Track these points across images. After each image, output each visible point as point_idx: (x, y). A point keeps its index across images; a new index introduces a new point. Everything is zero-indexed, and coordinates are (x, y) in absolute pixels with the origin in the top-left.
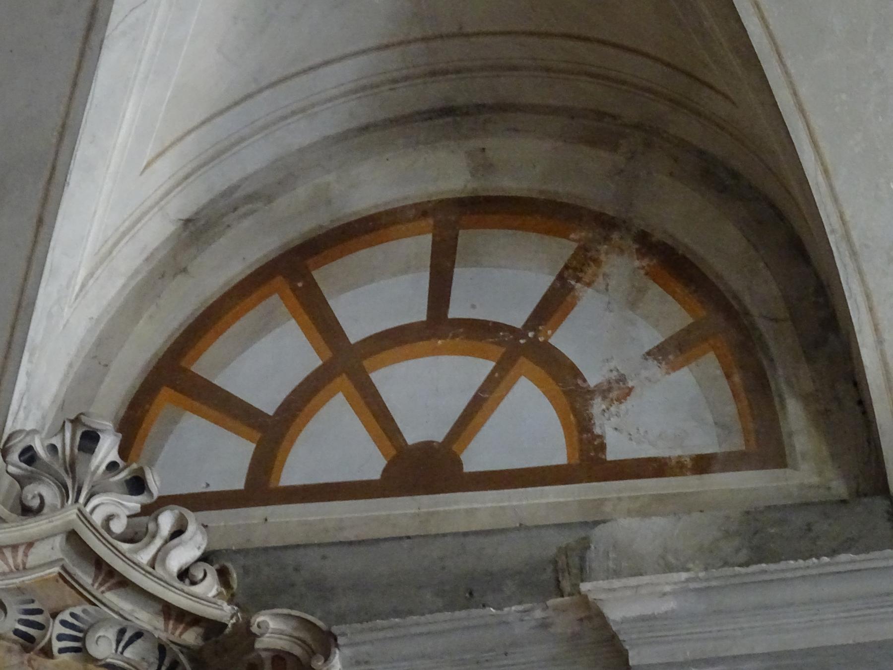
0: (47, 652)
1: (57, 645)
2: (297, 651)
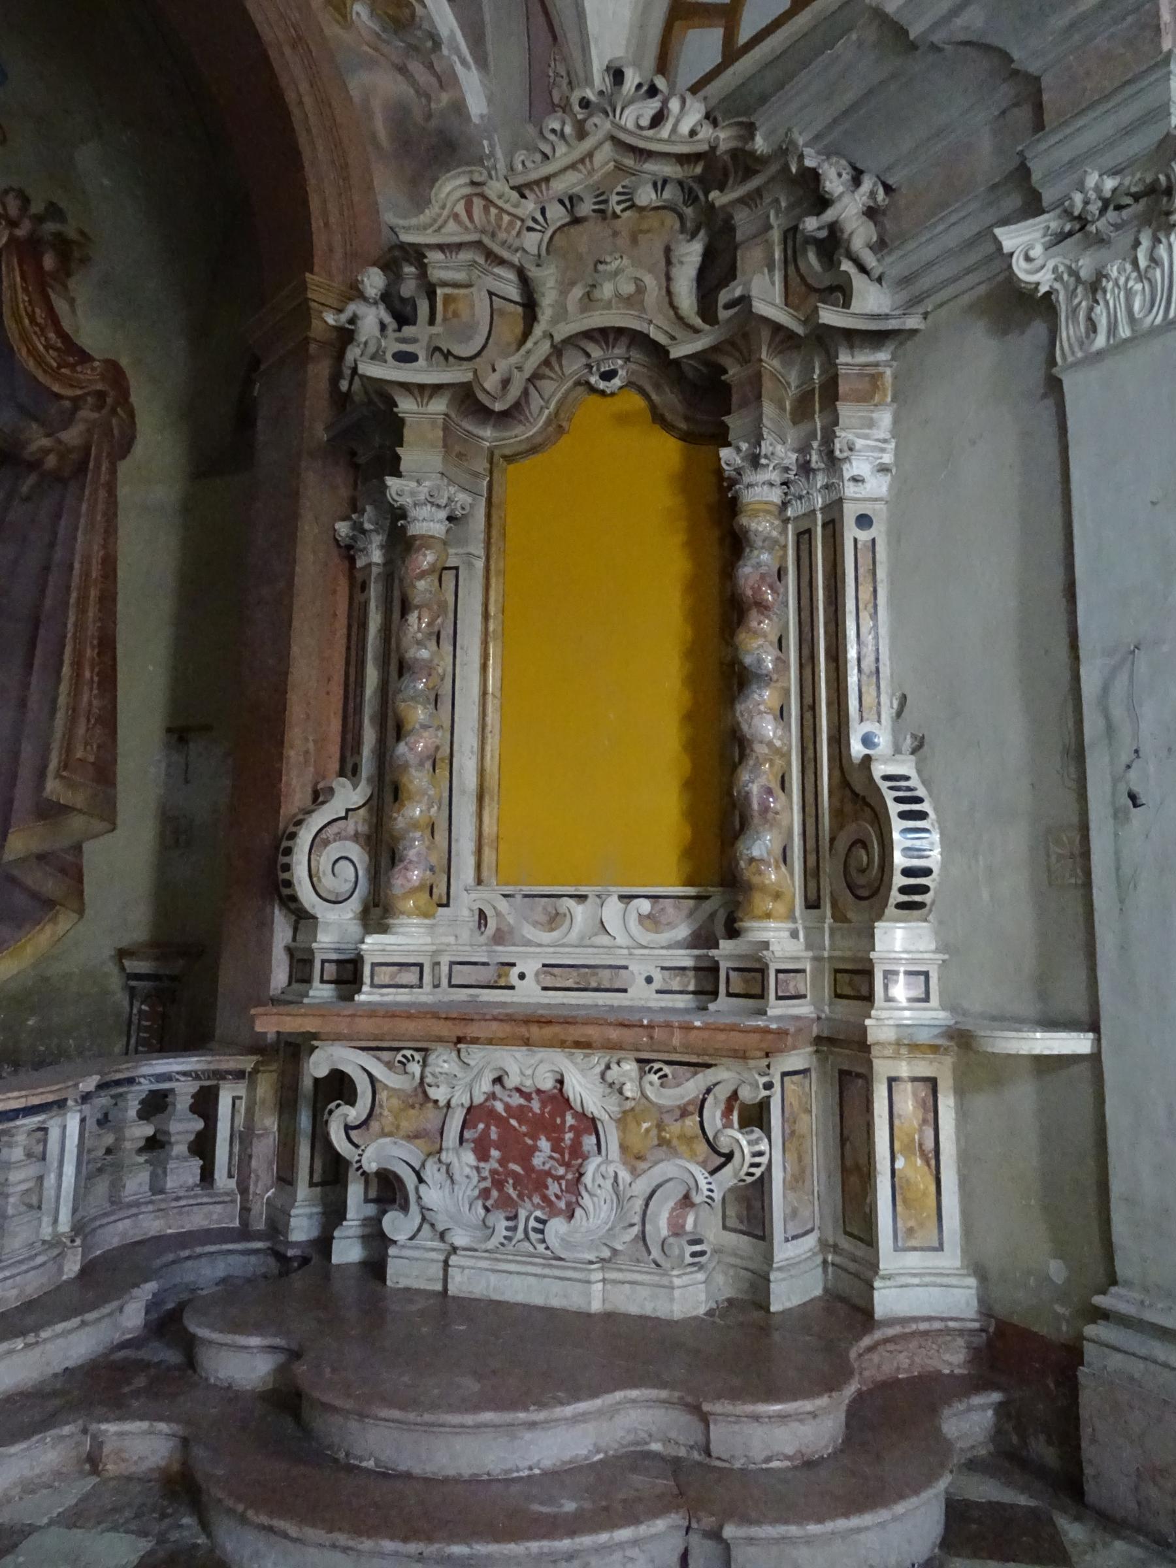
0: (615, 216)
1: (618, 209)
2: (740, 145)
